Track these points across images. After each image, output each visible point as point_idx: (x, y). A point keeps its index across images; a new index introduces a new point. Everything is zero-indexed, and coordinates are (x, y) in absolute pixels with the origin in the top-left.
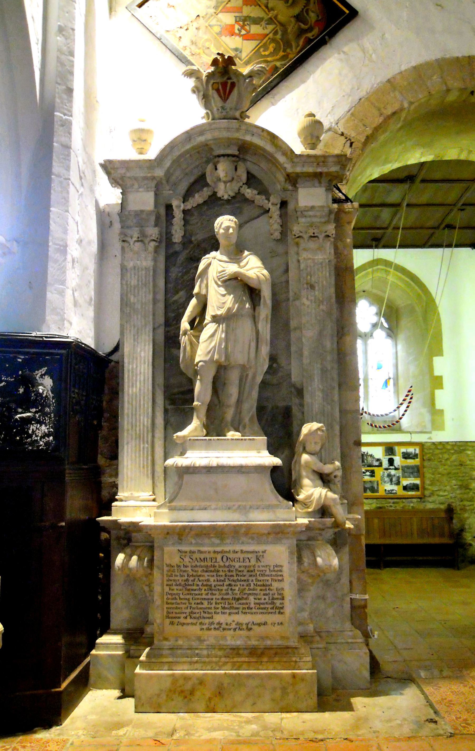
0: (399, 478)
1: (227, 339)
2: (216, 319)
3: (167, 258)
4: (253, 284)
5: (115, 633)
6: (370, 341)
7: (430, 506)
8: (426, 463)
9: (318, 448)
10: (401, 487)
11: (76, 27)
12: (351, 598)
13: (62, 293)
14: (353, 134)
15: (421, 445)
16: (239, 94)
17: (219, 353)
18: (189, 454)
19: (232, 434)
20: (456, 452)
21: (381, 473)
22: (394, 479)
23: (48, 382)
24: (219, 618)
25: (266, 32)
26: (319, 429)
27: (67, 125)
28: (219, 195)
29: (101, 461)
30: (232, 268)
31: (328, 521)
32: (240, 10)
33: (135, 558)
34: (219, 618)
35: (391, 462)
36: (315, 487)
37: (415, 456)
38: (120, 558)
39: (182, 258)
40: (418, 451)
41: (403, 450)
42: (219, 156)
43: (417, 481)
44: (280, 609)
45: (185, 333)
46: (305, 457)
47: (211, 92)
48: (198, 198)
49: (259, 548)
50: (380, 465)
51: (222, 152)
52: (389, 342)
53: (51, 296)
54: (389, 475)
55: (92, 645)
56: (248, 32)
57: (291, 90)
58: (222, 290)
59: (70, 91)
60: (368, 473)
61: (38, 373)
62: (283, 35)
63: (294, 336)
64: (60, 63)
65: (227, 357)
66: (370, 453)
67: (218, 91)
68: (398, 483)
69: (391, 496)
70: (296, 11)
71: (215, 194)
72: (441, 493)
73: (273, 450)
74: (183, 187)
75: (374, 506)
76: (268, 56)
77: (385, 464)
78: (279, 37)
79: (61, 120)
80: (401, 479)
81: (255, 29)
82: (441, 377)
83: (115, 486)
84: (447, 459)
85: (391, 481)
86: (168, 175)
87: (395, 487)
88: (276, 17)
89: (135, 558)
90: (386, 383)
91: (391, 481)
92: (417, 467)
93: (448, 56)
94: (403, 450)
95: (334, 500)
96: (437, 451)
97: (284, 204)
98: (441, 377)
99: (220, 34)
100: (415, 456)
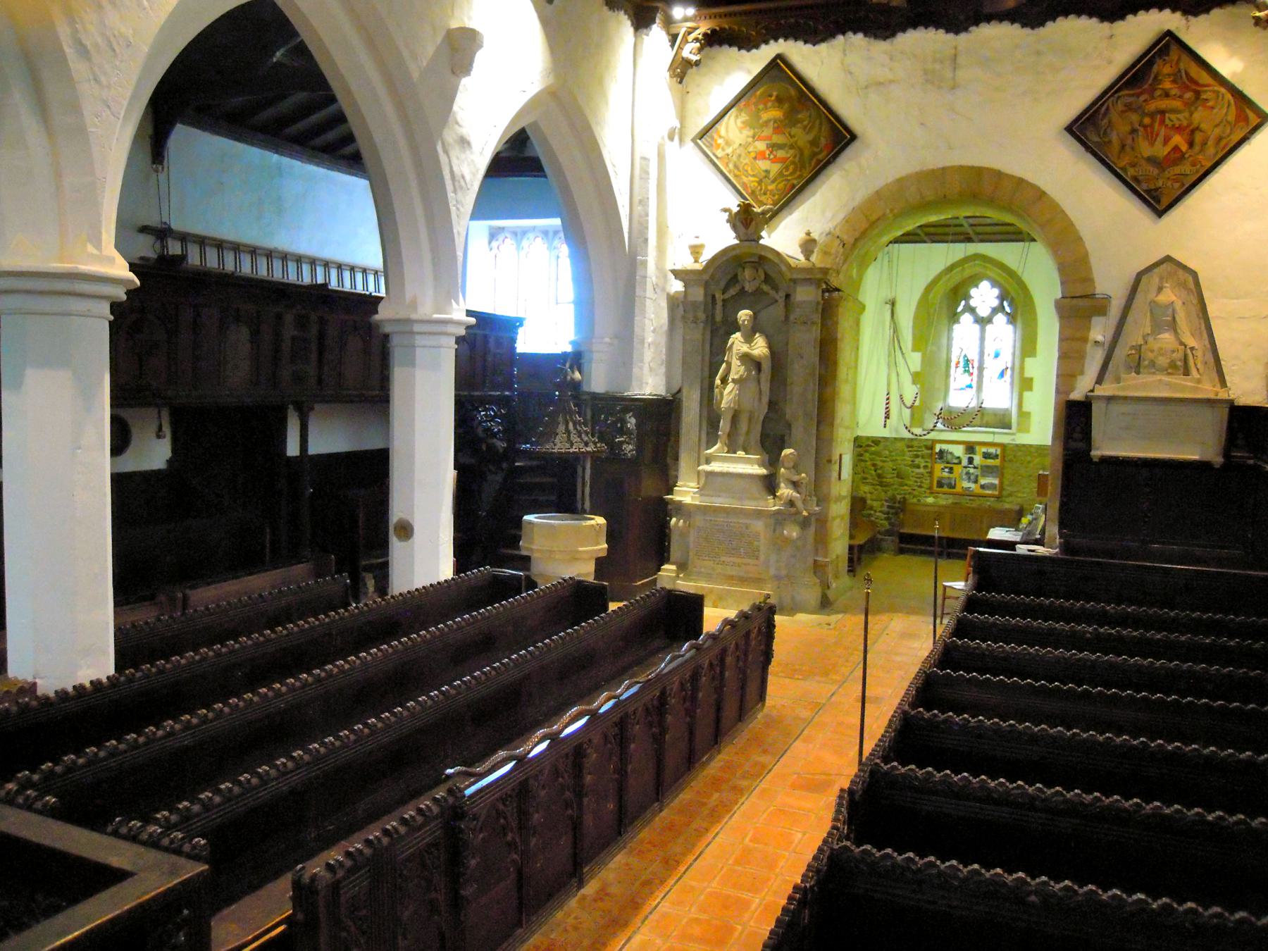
0: (977, 476)
1: (739, 394)
2: (734, 381)
3: (712, 332)
4: (758, 360)
5: (672, 564)
6: (989, 327)
7: (1007, 506)
8: (1006, 464)
9: (792, 464)
10: (979, 484)
11: (650, 196)
12: (815, 561)
13: (641, 368)
14: (845, 237)
15: (1003, 446)
16: (757, 224)
17: (734, 403)
18: (712, 464)
19: (741, 453)
20: (1040, 455)
21: (960, 471)
22: (972, 477)
23: (633, 421)
24: (723, 559)
25: (789, 155)
26: (791, 454)
27: (645, 263)
28: (746, 289)
29: (669, 460)
30: (745, 348)
31: (793, 510)
32: (769, 138)
33: (682, 521)
34: (723, 559)
35: (971, 461)
36: (787, 488)
37: (996, 456)
38: (674, 520)
39: (722, 331)
40: (999, 452)
41: (984, 450)
42: (746, 262)
43: (996, 481)
44: (757, 558)
45: (717, 388)
46: (782, 470)
47: (738, 224)
48: (732, 292)
49: (748, 521)
50: (960, 463)
51: (747, 260)
52: (1010, 327)
53: (635, 370)
54: (968, 473)
55: (659, 570)
56: (775, 156)
57: (803, 203)
58: (738, 363)
59: (646, 240)
60: (947, 470)
61: (628, 416)
62: (800, 158)
63: (788, 388)
64: (640, 223)
65: (739, 405)
66: (950, 450)
67: (742, 222)
68: (976, 482)
69: (967, 493)
70: (810, 137)
71: (743, 288)
72: (1019, 495)
73: (762, 465)
74: (722, 284)
75: (950, 501)
76: (787, 176)
77: (965, 462)
78: (797, 159)
79: (641, 260)
80: (979, 478)
81: (781, 154)
82: (1031, 380)
83: (677, 477)
84: (1029, 462)
85: (969, 478)
86: (712, 277)
87: (972, 486)
88: (796, 143)
89: (682, 521)
90: (1002, 374)
91: (969, 478)
92: (996, 467)
93: (925, 169)
94: (984, 450)
95: (797, 497)
96: (1020, 453)
97: (788, 296)
98: (1031, 380)
99: (755, 158)
100: (996, 456)
